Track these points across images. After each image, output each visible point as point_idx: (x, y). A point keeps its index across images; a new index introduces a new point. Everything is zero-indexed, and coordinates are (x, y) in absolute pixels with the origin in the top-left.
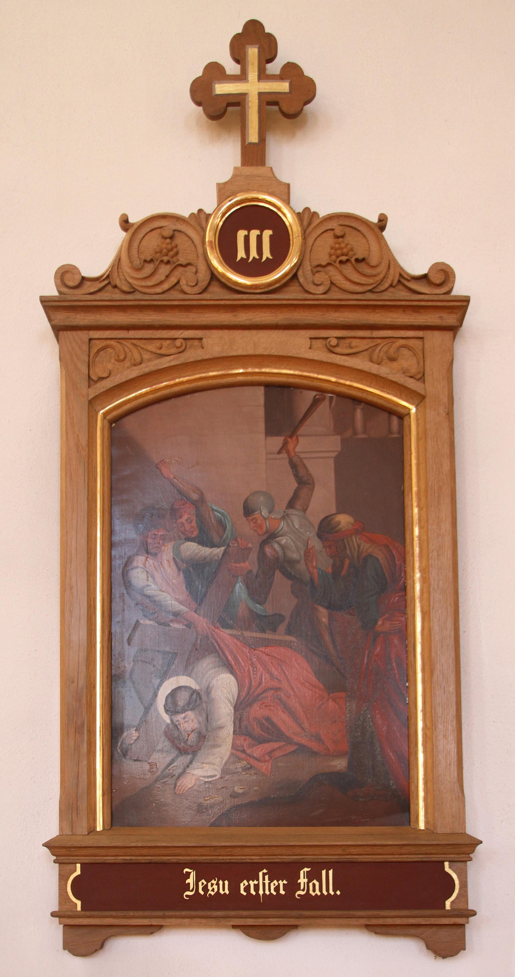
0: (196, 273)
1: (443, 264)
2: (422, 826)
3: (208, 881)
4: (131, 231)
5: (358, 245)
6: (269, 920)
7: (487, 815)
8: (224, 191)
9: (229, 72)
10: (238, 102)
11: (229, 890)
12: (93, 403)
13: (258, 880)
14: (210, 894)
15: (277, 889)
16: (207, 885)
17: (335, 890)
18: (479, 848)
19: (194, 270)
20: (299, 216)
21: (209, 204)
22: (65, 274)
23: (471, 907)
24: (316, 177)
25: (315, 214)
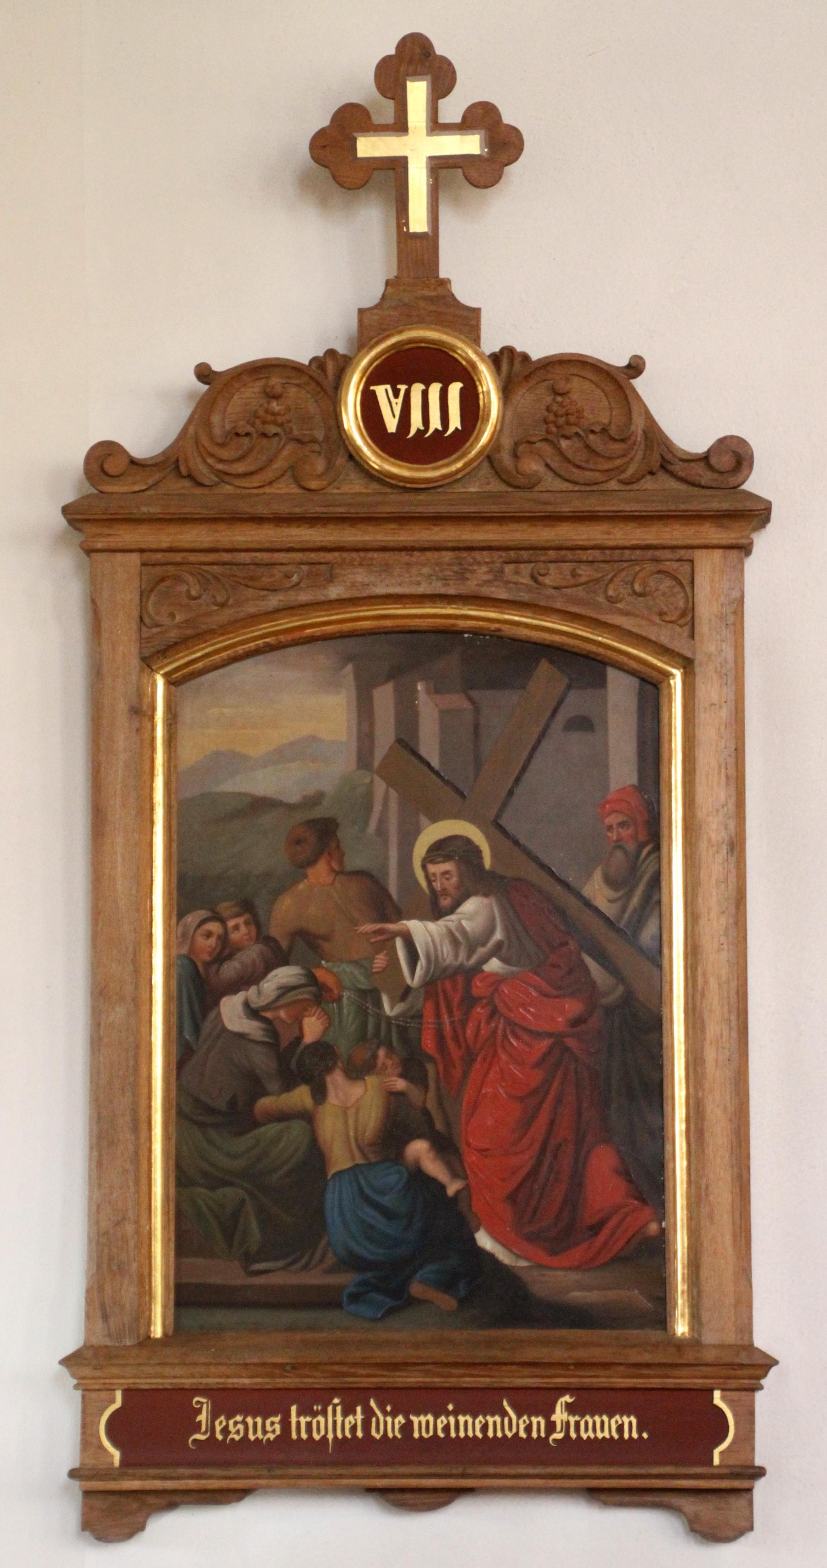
2: (681, 1328)
3: (228, 1418)
4: (621, 377)
5: (593, 405)
6: (416, 1477)
7: (779, 1321)
8: (370, 324)
9: (377, 119)
13: (355, 1413)
14: (233, 1439)
16: (227, 1426)
17: (640, 1432)
18: (773, 1371)
22: (104, 460)
23: (758, 1462)
24: (529, 283)
25: (525, 357)
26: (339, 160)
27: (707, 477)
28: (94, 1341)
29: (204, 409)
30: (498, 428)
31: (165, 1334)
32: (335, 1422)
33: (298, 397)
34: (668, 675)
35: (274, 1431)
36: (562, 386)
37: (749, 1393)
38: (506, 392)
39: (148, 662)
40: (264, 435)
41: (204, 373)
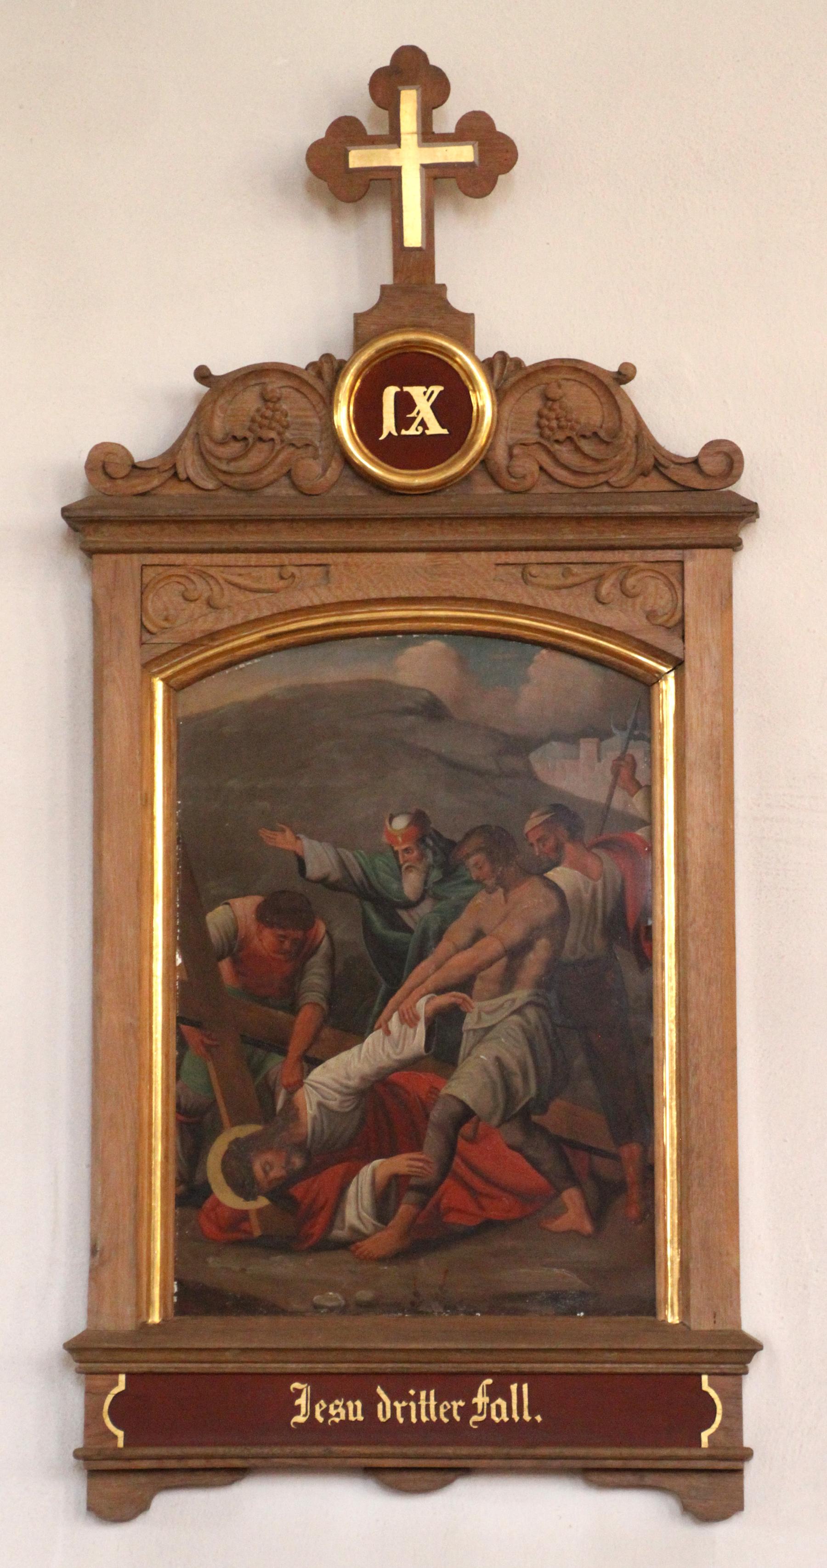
3: (328, 1402)
5: (587, 409)
6: (415, 1462)
7: (771, 1298)
8: (364, 328)
9: (370, 131)
11: (363, 1414)
15: (449, 1413)
16: (327, 1409)
17: (532, 1413)
20: (488, 366)
22: (105, 463)
24: (522, 291)
25: (518, 363)
26: (338, 173)
27: (697, 481)
28: (107, 1324)
29: (202, 412)
30: (493, 430)
31: (164, 1318)
32: (428, 1407)
33: (295, 405)
36: (554, 392)
37: (736, 1378)
38: (500, 394)
39: (149, 666)
40: (261, 439)
41: (202, 375)
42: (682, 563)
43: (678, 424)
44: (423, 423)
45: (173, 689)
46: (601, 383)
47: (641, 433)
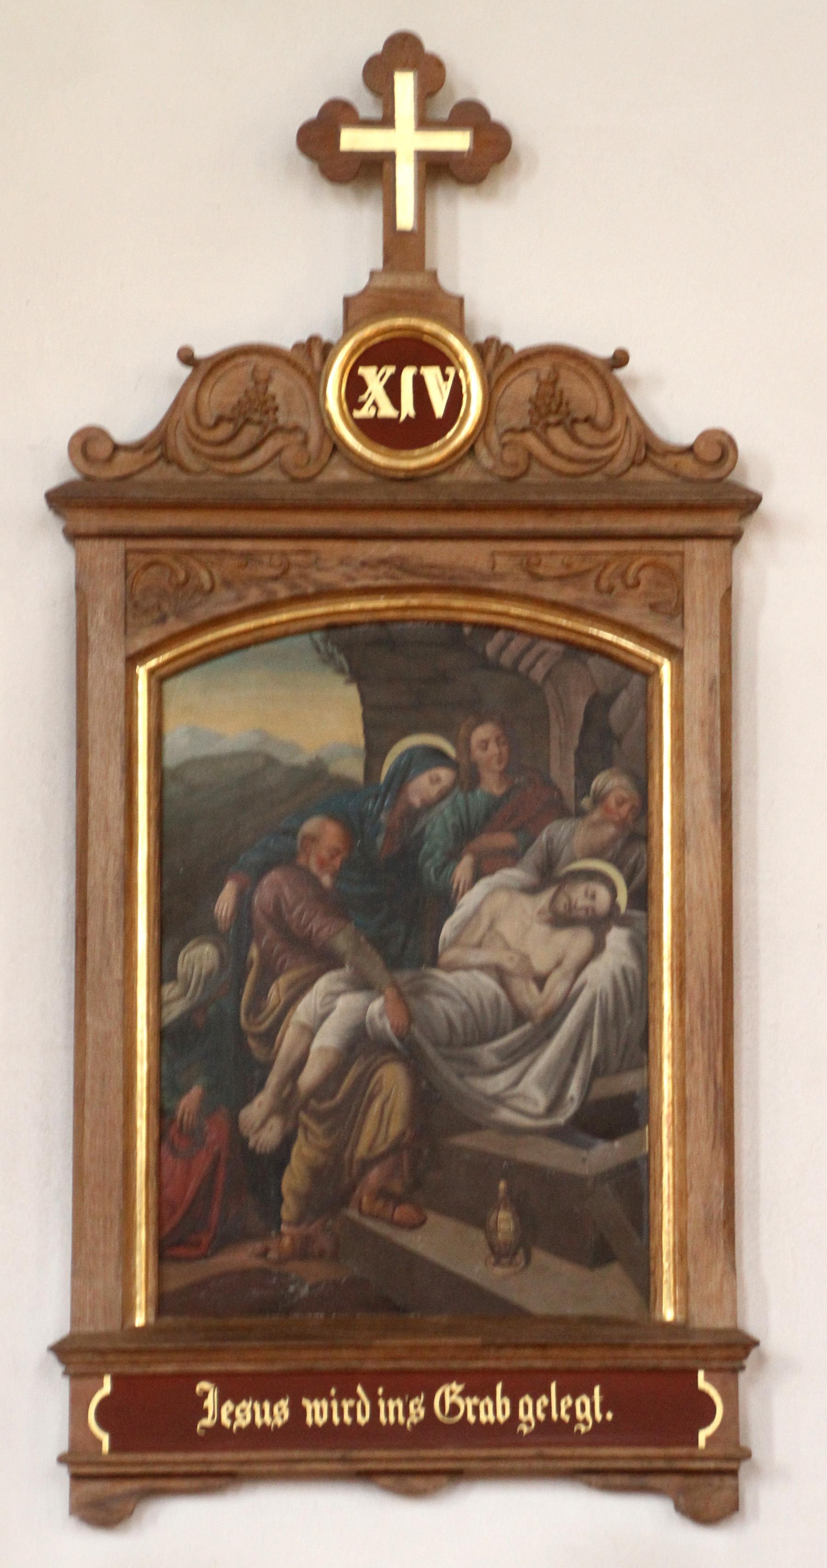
0: (305, 442)
1: (723, 433)
2: (669, 1314)
3: (236, 1402)
5: (580, 392)
8: (355, 310)
10: (375, 169)
12: (133, 660)
17: (604, 1411)
18: (754, 1353)
19: (300, 437)
20: (481, 351)
21: (328, 327)
22: (88, 444)
24: (519, 275)
25: (507, 347)
34: (657, 667)
35: (418, 1415)
41: (186, 357)
42: (682, 554)
43: (675, 413)
44: (374, 404)
45: (158, 680)
46: (596, 371)
47: (634, 418)
